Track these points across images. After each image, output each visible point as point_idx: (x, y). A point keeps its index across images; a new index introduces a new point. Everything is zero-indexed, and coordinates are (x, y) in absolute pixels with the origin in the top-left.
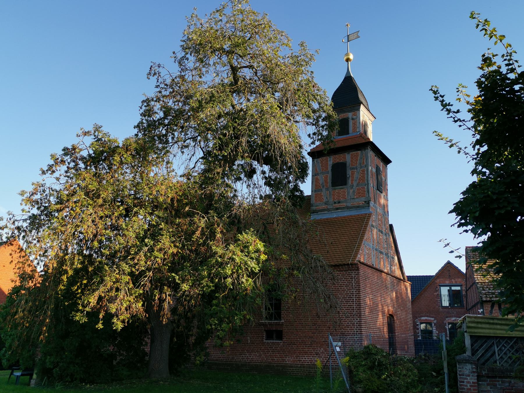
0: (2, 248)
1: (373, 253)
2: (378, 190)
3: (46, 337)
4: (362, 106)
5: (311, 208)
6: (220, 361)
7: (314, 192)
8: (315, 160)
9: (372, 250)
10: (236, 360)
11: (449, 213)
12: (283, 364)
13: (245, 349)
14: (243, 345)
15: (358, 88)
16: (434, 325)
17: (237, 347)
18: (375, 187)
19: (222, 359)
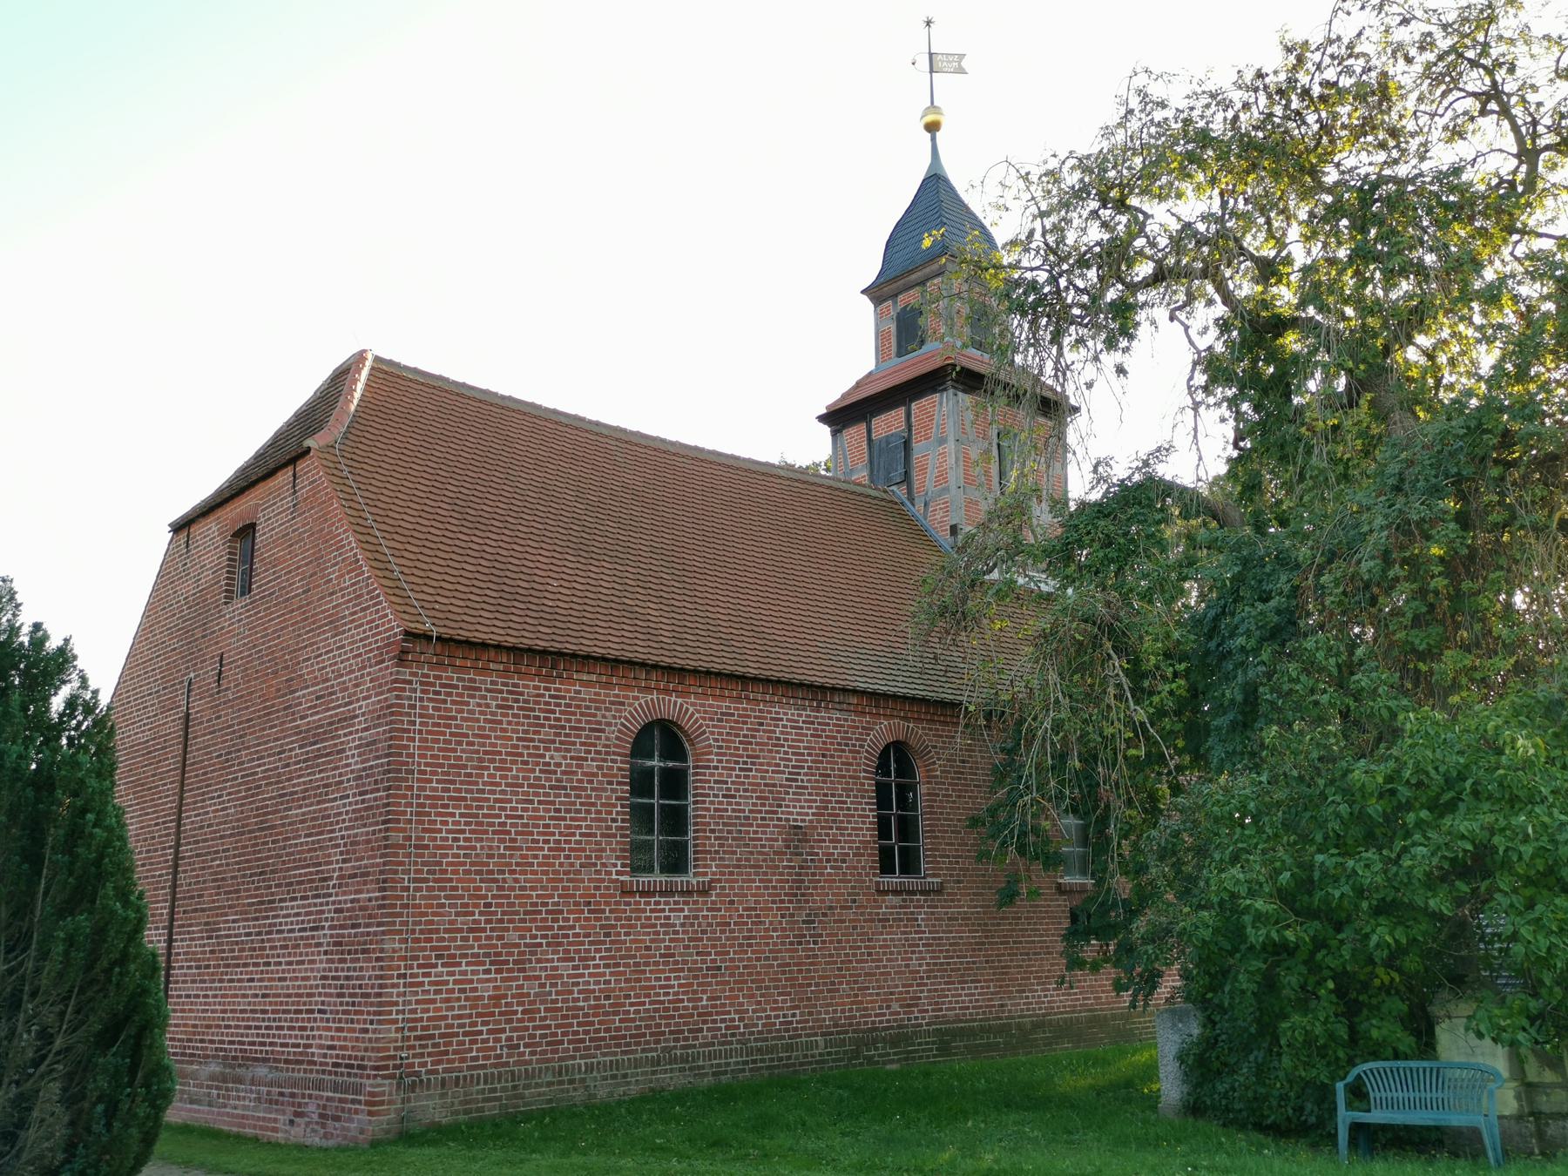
0: (1565, 1109)
6: (966, 1021)
10: (1010, 1011)
12: (1118, 1008)
13: (1031, 972)
14: (1023, 960)
17: (1009, 967)
19: (971, 1014)
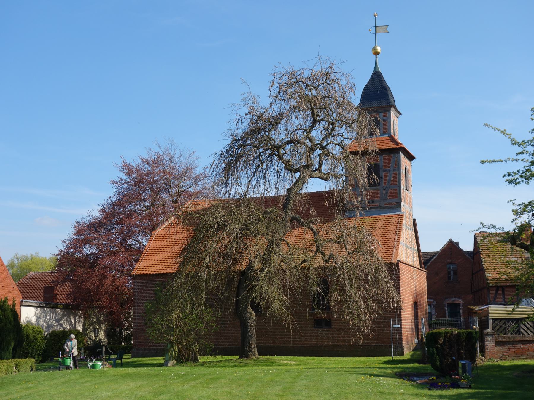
3: (127, 323)
4: (392, 108)
11: (401, 114)
15: (388, 88)
16: (433, 307)
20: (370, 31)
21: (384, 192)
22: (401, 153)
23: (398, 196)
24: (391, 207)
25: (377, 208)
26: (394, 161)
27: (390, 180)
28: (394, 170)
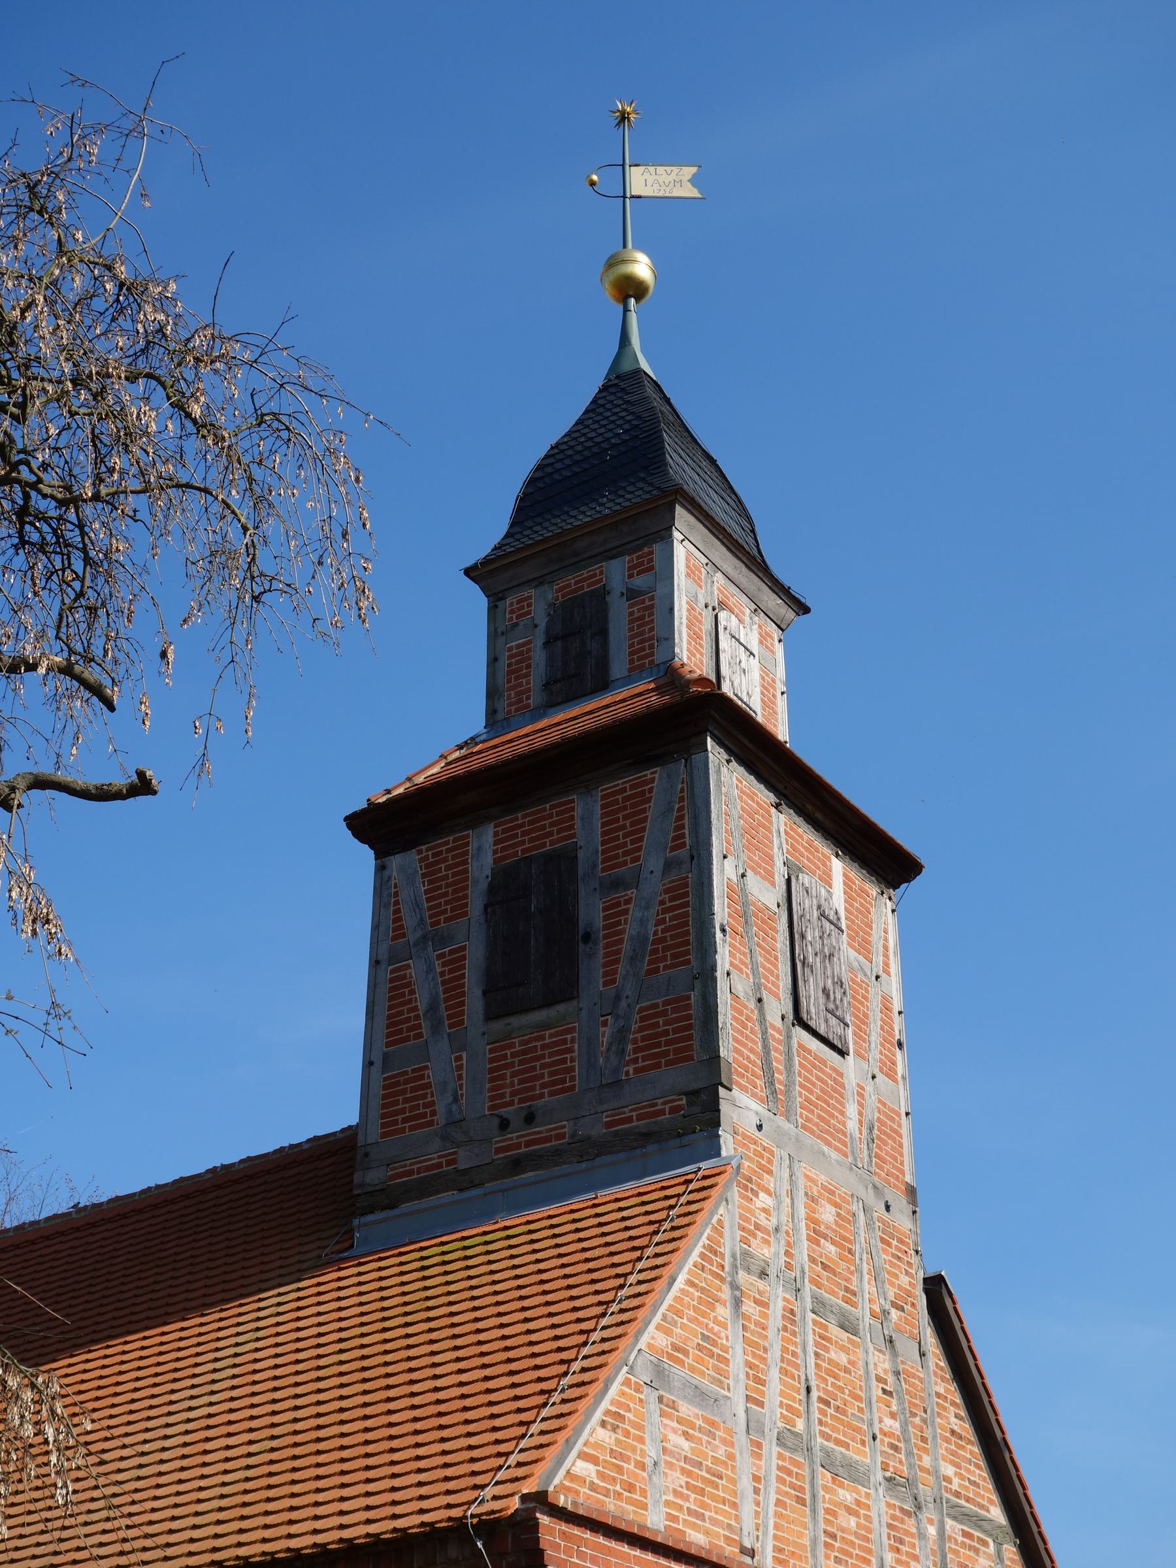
1: (745, 1465)
2: (800, 1020)
4: (682, 517)
5: (357, 1178)
7: (376, 1070)
8: (395, 862)
9: (741, 1439)
18: (778, 1007)
20: (593, 184)
21: (606, 1034)
22: (710, 742)
23: (696, 1043)
24: (647, 1137)
25: (554, 1157)
26: (671, 809)
27: (646, 939)
28: (668, 866)
